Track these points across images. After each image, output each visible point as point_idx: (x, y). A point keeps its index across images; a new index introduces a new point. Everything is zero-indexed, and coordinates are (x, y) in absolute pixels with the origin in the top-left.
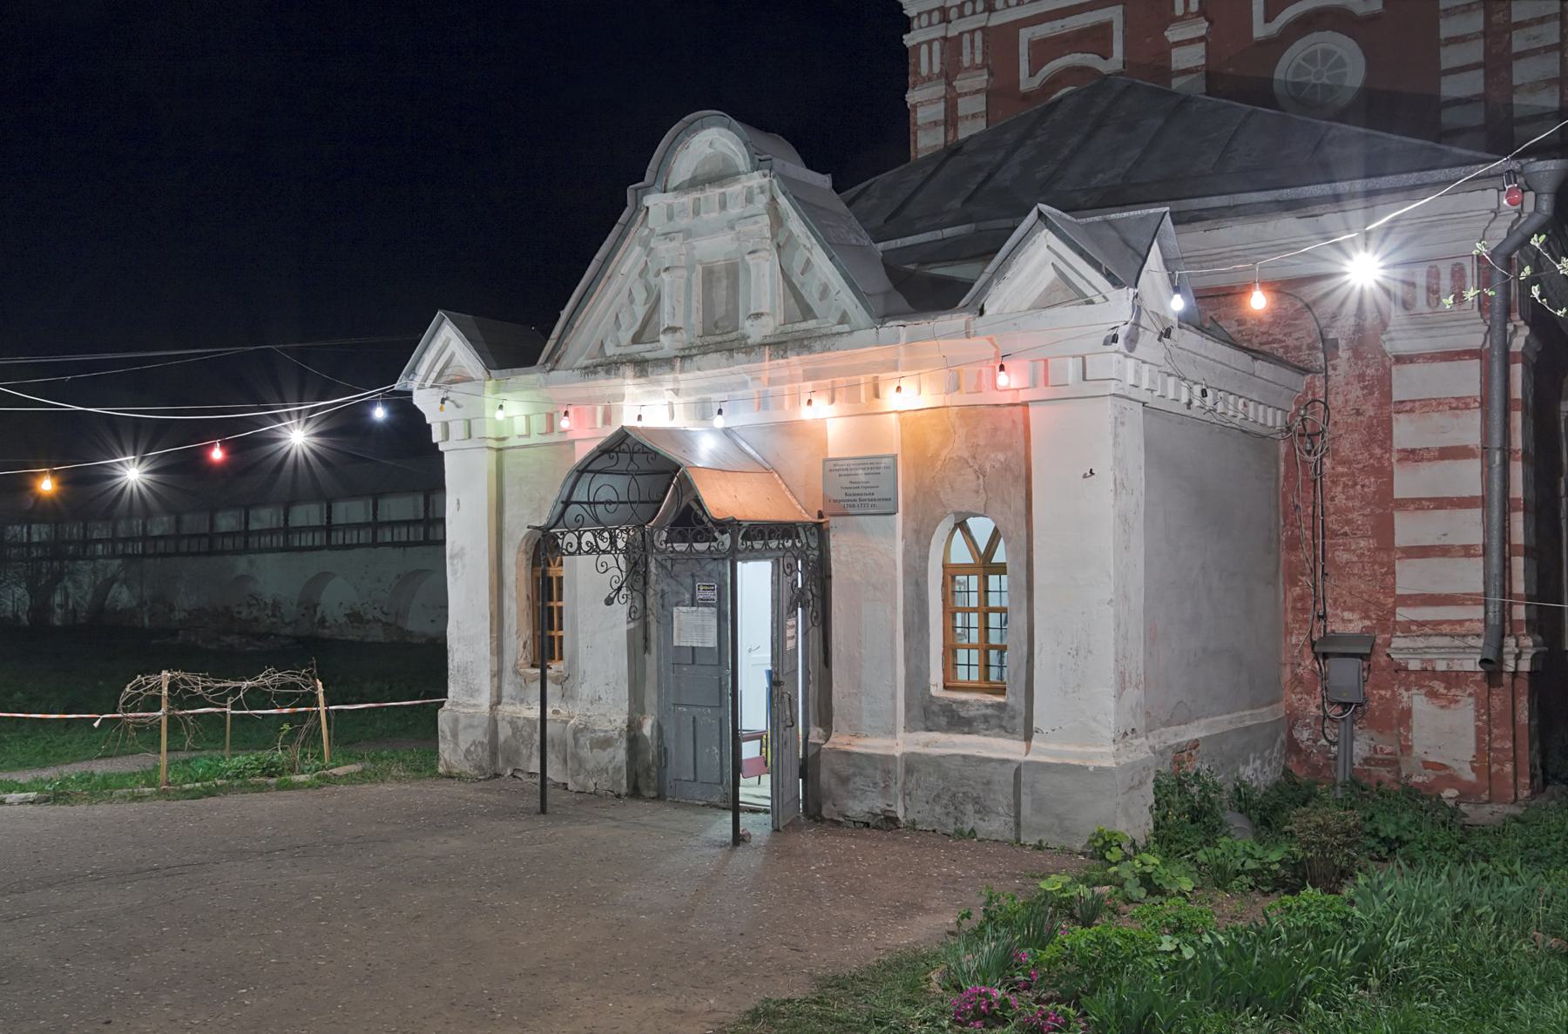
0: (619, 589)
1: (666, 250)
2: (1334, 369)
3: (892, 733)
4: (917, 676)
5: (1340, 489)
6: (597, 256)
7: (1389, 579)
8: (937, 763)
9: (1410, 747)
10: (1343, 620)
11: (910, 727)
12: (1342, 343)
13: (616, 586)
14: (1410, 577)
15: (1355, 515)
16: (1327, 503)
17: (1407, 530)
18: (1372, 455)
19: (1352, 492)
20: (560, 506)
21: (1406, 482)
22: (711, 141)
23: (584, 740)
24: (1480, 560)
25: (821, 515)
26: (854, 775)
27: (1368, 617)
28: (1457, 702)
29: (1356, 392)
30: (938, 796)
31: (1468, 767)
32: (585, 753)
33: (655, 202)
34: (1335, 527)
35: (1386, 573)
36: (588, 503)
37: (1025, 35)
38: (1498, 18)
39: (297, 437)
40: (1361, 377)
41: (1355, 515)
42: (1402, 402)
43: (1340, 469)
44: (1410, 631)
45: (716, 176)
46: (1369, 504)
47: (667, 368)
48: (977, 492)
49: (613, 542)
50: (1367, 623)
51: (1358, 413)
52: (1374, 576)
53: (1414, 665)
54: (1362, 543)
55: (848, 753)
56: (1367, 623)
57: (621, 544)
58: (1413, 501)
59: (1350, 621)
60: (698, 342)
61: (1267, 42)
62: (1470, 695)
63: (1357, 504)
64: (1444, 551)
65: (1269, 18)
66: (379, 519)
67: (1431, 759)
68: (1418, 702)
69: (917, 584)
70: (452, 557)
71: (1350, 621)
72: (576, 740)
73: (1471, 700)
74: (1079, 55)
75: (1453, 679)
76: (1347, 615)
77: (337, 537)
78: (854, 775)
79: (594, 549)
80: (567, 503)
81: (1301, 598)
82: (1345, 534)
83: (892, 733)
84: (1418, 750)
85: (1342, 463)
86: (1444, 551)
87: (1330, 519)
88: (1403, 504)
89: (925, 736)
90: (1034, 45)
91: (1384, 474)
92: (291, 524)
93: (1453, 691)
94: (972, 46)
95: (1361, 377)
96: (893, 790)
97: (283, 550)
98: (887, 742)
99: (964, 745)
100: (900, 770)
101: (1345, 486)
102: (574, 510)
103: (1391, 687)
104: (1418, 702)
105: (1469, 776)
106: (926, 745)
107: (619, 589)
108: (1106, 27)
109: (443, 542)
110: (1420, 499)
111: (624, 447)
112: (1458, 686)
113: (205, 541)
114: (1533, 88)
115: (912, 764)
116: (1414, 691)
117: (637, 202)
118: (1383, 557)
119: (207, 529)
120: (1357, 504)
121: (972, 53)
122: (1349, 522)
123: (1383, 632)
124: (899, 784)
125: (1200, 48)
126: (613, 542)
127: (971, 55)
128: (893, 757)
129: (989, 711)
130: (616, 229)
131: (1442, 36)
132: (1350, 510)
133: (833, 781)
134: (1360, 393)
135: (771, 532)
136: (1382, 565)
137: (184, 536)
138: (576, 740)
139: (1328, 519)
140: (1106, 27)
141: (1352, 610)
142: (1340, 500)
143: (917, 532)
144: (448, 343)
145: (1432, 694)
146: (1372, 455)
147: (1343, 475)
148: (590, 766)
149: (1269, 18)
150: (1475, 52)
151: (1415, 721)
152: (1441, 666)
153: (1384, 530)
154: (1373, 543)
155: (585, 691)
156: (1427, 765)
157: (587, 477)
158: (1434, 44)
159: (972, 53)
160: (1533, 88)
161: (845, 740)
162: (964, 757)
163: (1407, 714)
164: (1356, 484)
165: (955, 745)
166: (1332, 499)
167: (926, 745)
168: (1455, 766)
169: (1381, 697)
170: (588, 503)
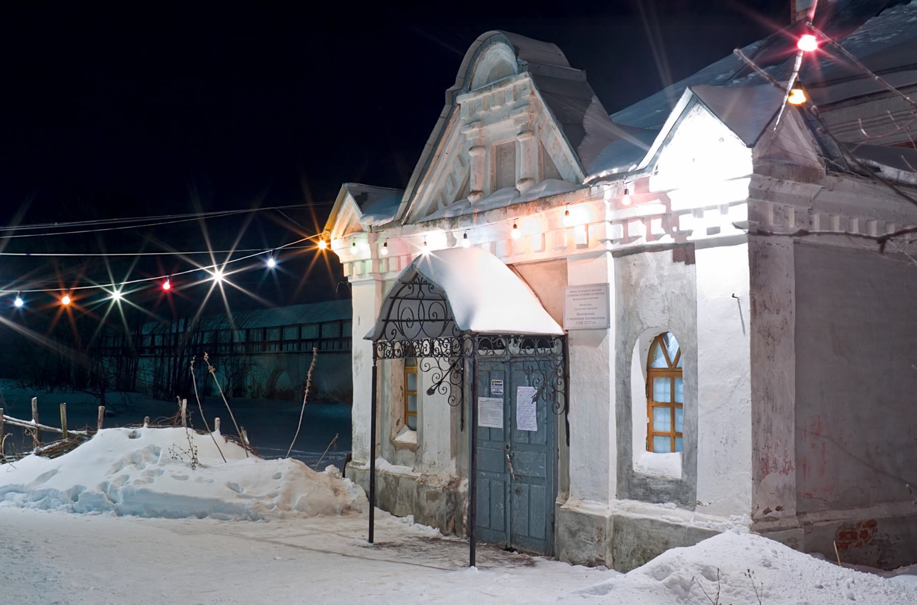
1: (471, 133)
4: (625, 456)
6: (429, 141)
8: (634, 524)
11: (619, 496)
13: (437, 381)
22: (497, 53)
23: (423, 495)
26: (579, 530)
30: (634, 551)
32: (423, 503)
33: (464, 100)
36: (398, 321)
39: (218, 276)
45: (499, 77)
47: (469, 221)
48: (663, 312)
55: (577, 514)
66: (303, 337)
69: (624, 383)
70: (356, 358)
72: (419, 493)
78: (579, 530)
80: (387, 321)
83: (605, 499)
89: (627, 503)
92: (344, 335)
96: (603, 544)
98: (602, 506)
99: (656, 512)
100: (609, 527)
102: (391, 326)
106: (628, 510)
109: (351, 352)
113: (336, 344)
115: (618, 524)
117: (453, 100)
119: (337, 335)
124: (608, 540)
128: (603, 519)
129: (670, 486)
130: (440, 121)
133: (566, 534)
137: (325, 340)
138: (419, 493)
143: (625, 343)
144: (347, 210)
148: (426, 512)
155: (426, 457)
161: (576, 502)
162: (652, 521)
165: (646, 512)
167: (628, 510)
170: (398, 321)
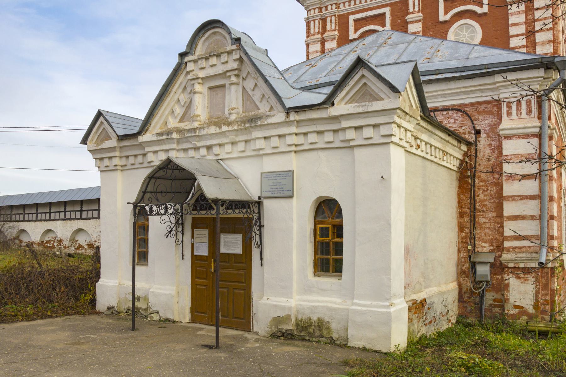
0: (171, 231)
2: (479, 142)
3: (289, 295)
5: (481, 192)
7: (501, 230)
9: (508, 299)
10: (482, 247)
12: (482, 131)
13: (169, 230)
14: (509, 228)
15: (487, 203)
16: (476, 198)
17: (509, 209)
18: (494, 178)
19: (486, 193)
20: (142, 194)
21: (509, 189)
24: (538, 222)
25: (259, 198)
27: (492, 245)
28: (528, 280)
29: (488, 151)
31: (531, 307)
34: (479, 208)
35: (500, 227)
37: (352, 18)
38: (530, 17)
40: (490, 145)
41: (487, 203)
42: (506, 156)
43: (481, 184)
44: (509, 251)
46: (493, 198)
49: (166, 211)
50: (492, 248)
51: (489, 160)
52: (495, 228)
53: (511, 265)
54: (490, 215)
56: (492, 248)
57: (170, 211)
58: (511, 197)
59: (485, 247)
60: (207, 121)
61: (445, 22)
62: (533, 277)
63: (488, 198)
64: (523, 218)
65: (446, 13)
67: (517, 304)
68: (512, 281)
71: (485, 247)
73: (534, 280)
74: (372, 26)
75: (526, 271)
76: (484, 244)
77: (84, 215)
79: (158, 214)
81: (465, 238)
82: (483, 211)
84: (512, 300)
85: (482, 181)
86: (523, 218)
87: (478, 204)
88: (508, 198)
90: (356, 21)
91: (499, 186)
93: (526, 276)
94: (331, 22)
95: (490, 145)
97: (63, 220)
101: (484, 190)
102: (148, 195)
103: (501, 274)
104: (512, 281)
105: (531, 310)
107: (171, 231)
108: (384, 14)
110: (514, 196)
111: (169, 166)
112: (528, 273)
114: (543, 44)
116: (511, 276)
118: (498, 220)
120: (488, 198)
121: (331, 25)
122: (485, 206)
123: (498, 251)
125: (420, 24)
126: (166, 211)
127: (331, 25)
131: (510, 23)
132: (485, 200)
134: (489, 151)
135: (236, 205)
136: (498, 223)
139: (477, 205)
140: (384, 14)
141: (485, 242)
142: (482, 196)
145: (518, 277)
146: (494, 178)
147: (482, 186)
149: (446, 13)
150: (522, 29)
151: (510, 289)
152: (522, 265)
153: (499, 208)
154: (494, 214)
156: (516, 307)
157: (153, 180)
158: (507, 26)
159: (331, 25)
160: (543, 44)
163: (508, 285)
164: (488, 190)
166: (478, 196)
168: (527, 307)
169: (497, 279)
